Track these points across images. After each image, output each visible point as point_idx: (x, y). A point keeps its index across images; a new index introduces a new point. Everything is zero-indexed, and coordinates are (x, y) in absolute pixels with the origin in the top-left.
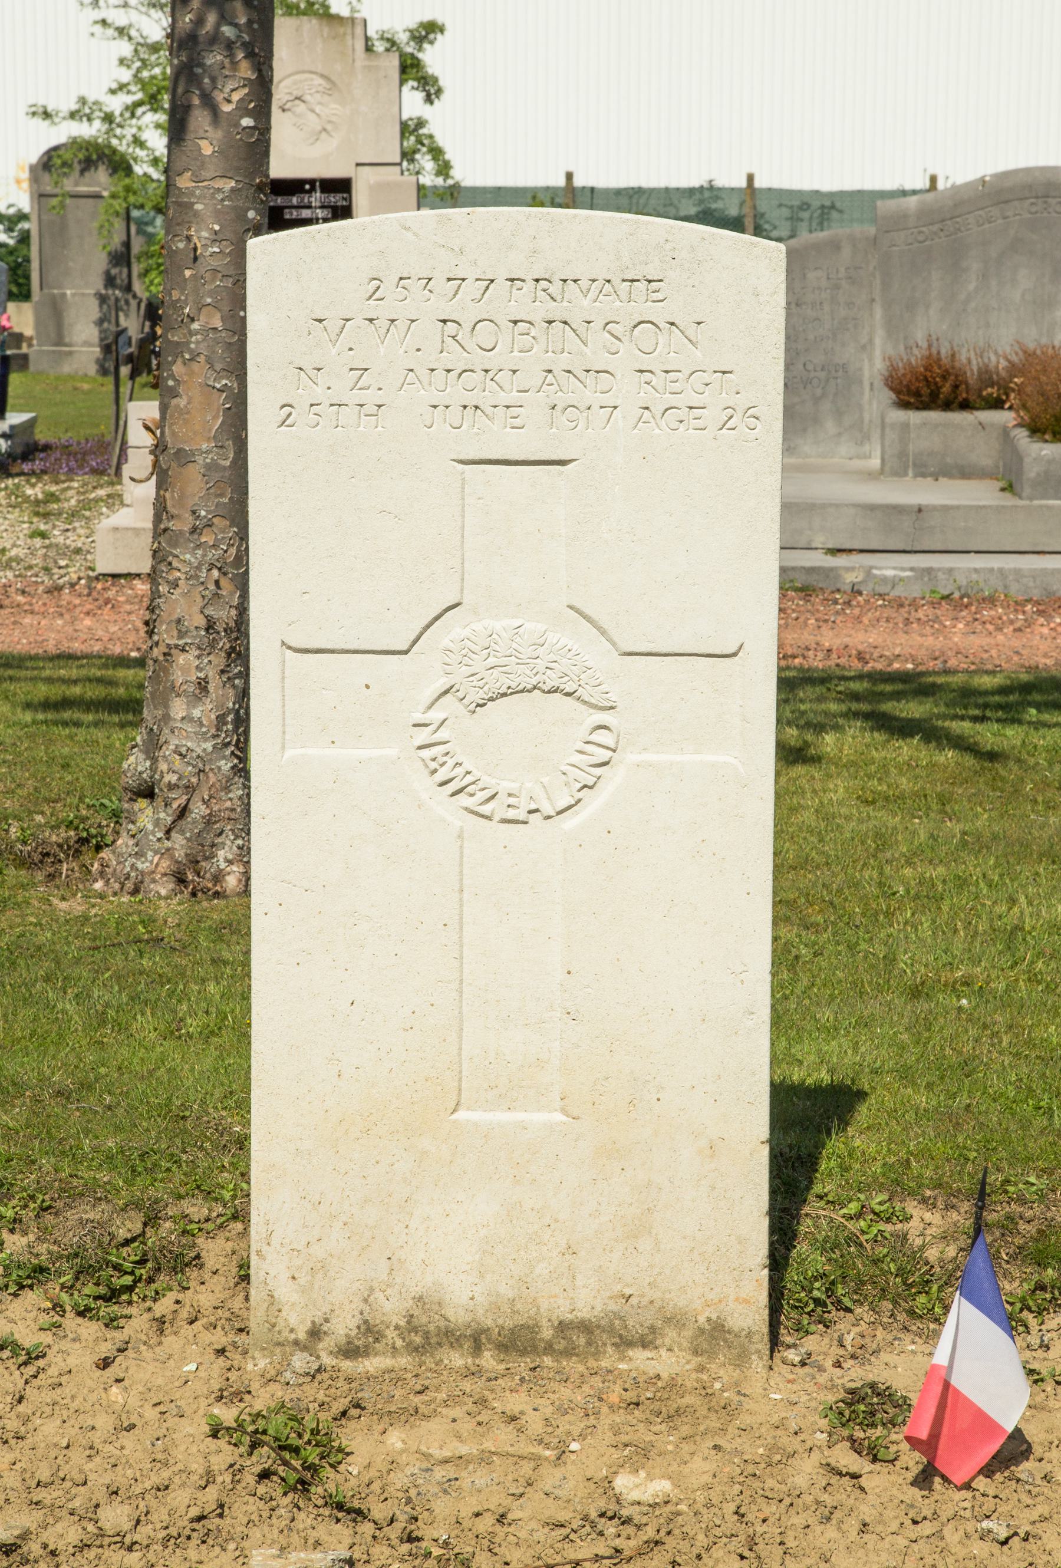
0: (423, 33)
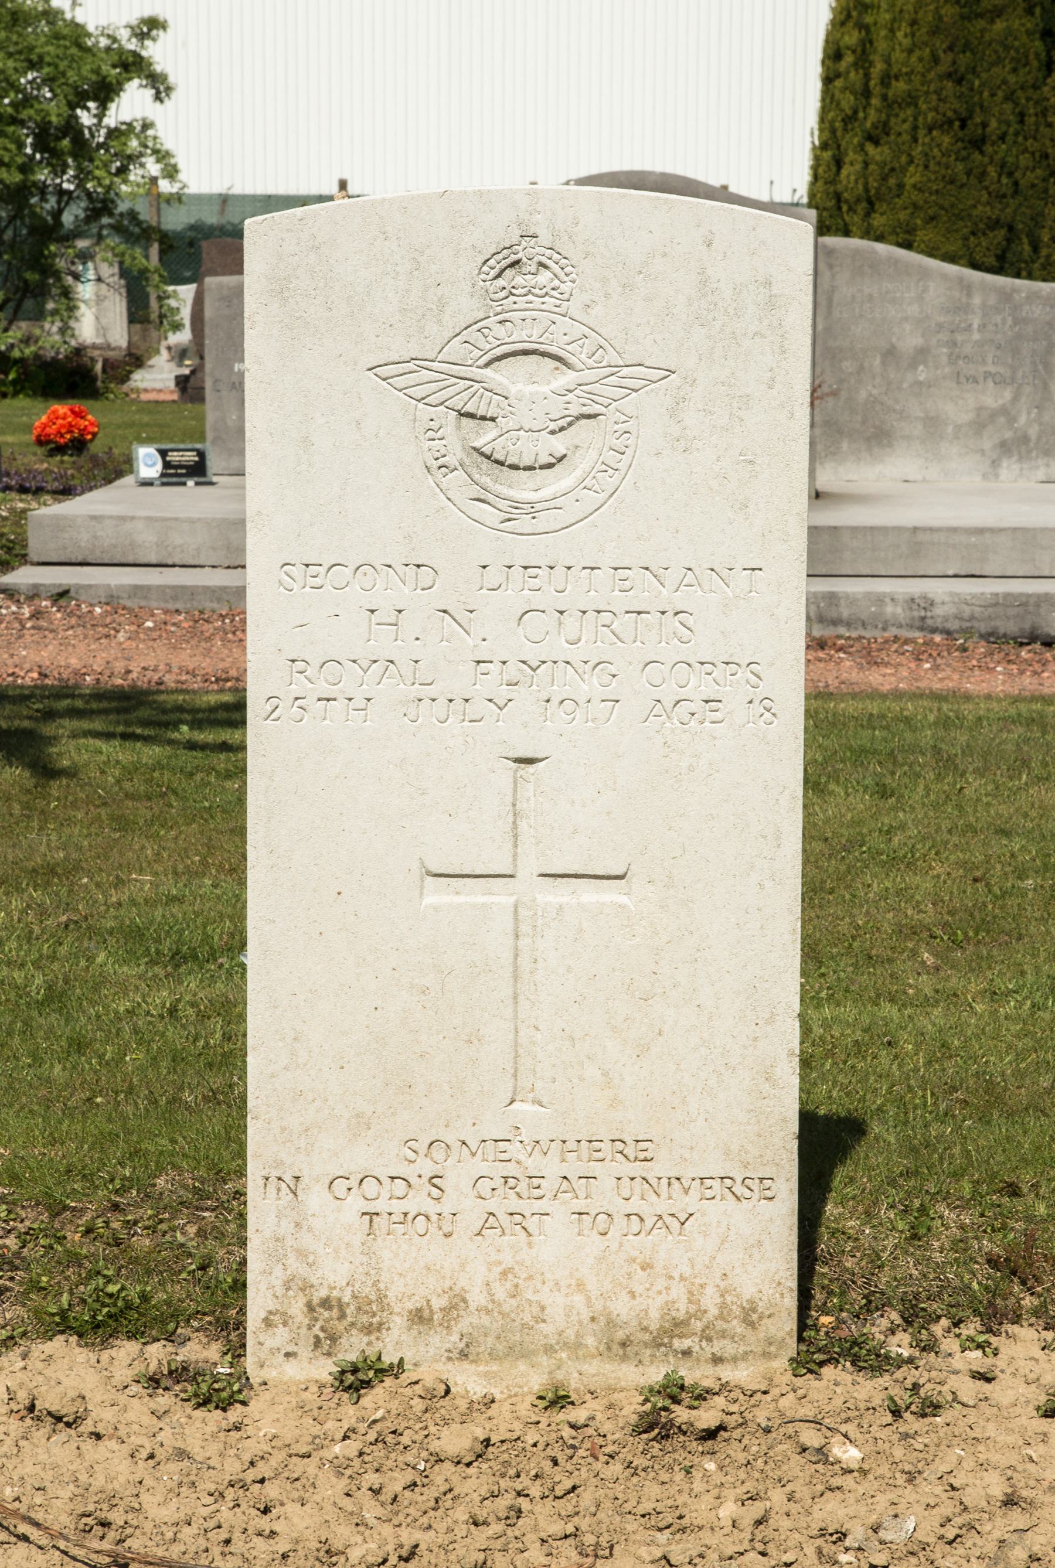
0: (145, 29)
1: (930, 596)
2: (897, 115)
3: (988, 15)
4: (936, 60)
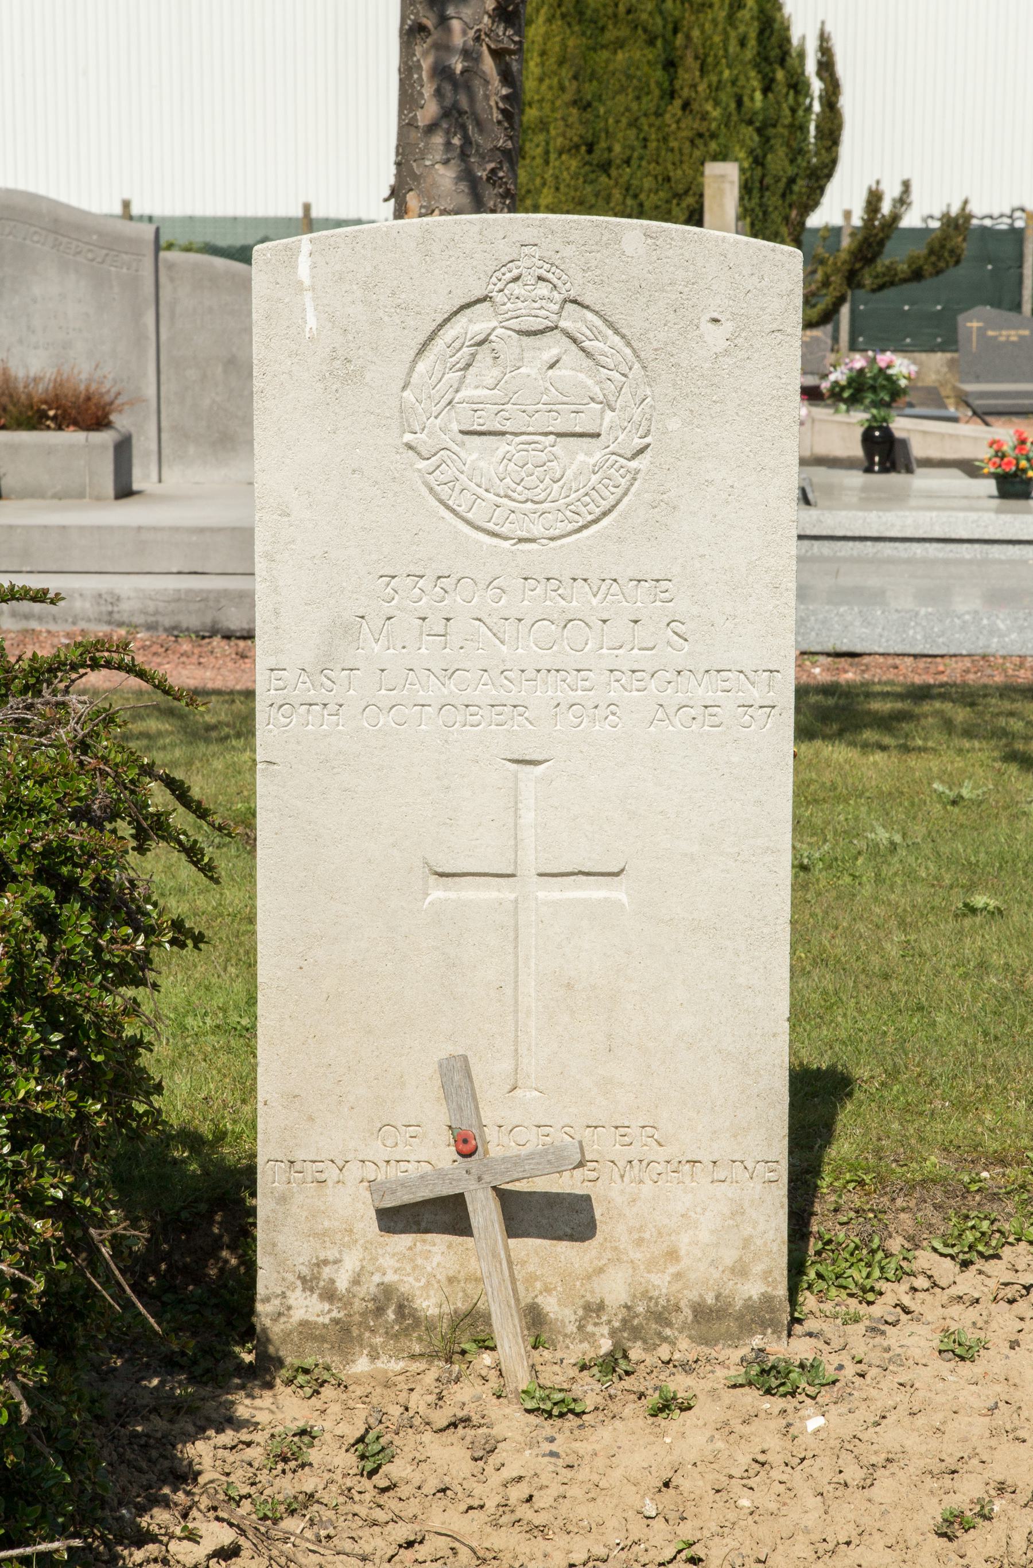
1: (117, 591)
2: (531, 140)
3: (612, 46)
4: (562, 88)
